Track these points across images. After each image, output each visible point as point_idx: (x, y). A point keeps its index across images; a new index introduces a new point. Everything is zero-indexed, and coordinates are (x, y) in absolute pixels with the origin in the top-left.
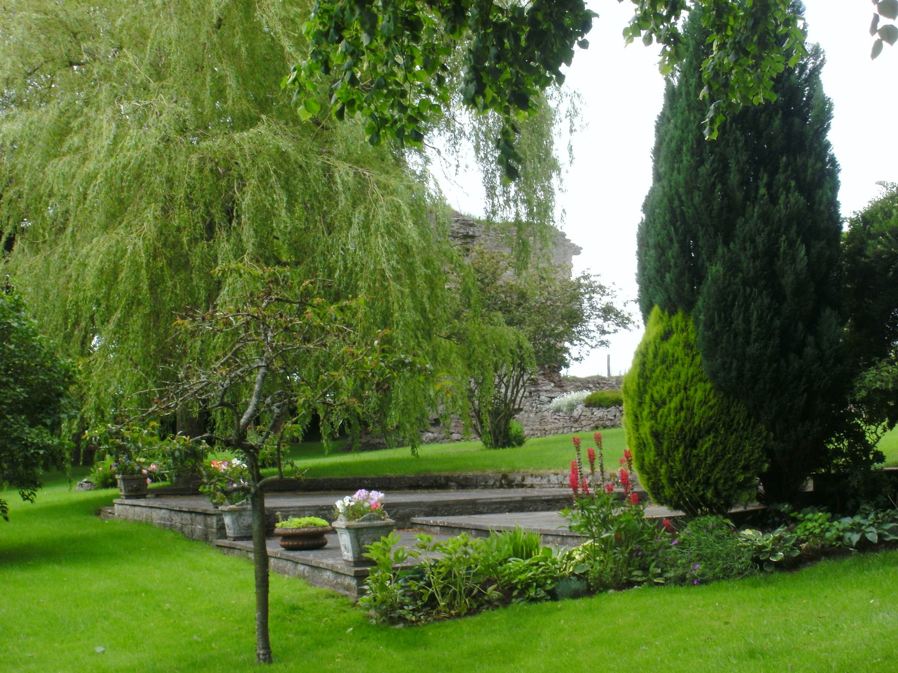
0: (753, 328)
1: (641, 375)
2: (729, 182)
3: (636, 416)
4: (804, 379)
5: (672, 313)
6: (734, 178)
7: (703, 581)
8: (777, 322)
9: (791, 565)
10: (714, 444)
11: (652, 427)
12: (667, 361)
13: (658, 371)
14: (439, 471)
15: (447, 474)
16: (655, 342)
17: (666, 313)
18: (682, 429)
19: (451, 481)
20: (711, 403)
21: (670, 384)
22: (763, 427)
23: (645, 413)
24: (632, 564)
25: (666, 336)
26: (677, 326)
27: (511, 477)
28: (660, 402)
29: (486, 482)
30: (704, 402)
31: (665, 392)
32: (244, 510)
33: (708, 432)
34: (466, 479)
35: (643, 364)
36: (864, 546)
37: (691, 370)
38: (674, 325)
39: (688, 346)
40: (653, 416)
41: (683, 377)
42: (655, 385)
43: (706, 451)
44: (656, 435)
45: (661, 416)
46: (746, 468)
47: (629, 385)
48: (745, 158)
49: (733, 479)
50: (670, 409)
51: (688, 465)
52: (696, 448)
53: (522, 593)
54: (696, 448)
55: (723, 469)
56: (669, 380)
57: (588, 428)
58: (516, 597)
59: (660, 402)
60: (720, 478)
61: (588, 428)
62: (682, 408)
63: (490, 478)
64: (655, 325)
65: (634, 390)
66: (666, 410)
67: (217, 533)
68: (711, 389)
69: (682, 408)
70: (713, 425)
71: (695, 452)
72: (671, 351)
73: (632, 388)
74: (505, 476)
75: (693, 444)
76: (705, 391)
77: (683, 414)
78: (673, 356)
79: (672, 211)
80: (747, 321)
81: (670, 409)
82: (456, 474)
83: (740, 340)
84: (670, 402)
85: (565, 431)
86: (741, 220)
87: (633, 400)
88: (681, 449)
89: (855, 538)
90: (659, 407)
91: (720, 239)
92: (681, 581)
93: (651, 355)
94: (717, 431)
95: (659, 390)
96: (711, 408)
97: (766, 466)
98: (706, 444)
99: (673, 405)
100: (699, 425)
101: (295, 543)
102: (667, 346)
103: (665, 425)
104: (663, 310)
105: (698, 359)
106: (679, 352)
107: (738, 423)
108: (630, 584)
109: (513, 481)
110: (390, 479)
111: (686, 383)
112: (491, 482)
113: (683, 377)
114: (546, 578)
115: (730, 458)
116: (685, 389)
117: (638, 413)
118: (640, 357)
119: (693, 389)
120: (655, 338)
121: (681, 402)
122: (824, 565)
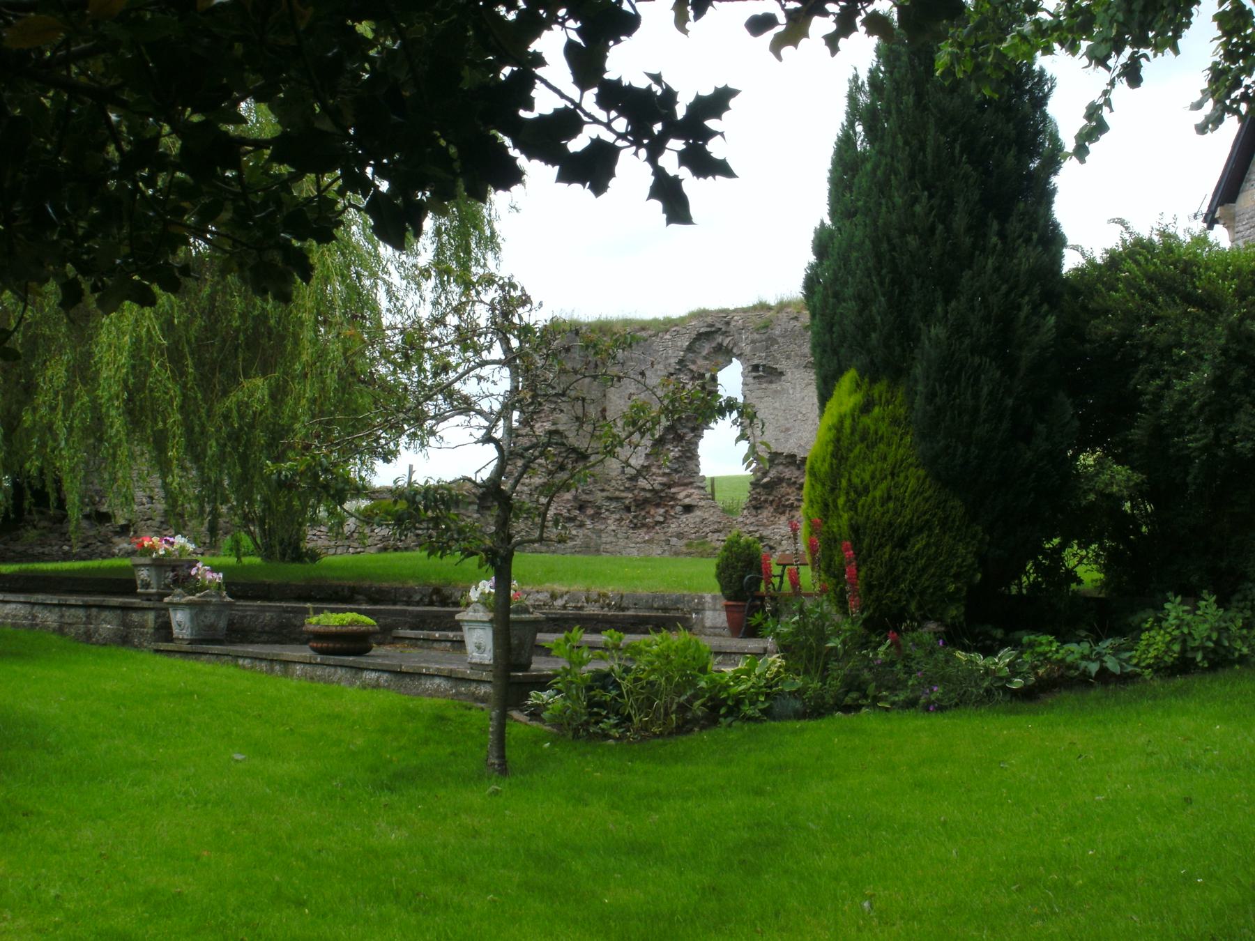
0: (983, 406)
1: (834, 455)
2: (954, 225)
3: (826, 505)
4: (1033, 475)
5: (873, 381)
6: (960, 221)
7: (941, 709)
8: (1010, 402)
9: (1029, 695)
10: (927, 545)
11: (851, 519)
12: (868, 439)
13: (856, 451)
14: (338, 579)
15: (351, 583)
16: (853, 416)
17: (866, 380)
18: (890, 524)
19: (359, 593)
20: (927, 494)
21: (872, 467)
22: (979, 528)
23: (841, 501)
24: (833, 689)
25: (866, 408)
26: (880, 397)
27: (446, 591)
28: (860, 488)
29: (410, 597)
30: (915, 494)
31: (867, 477)
32: (208, 603)
33: (920, 531)
34: (380, 591)
35: (837, 440)
36: (1104, 676)
37: (901, 451)
38: (876, 395)
39: (895, 422)
40: (852, 505)
41: (890, 459)
42: (853, 467)
43: (917, 553)
44: (855, 529)
45: (863, 506)
46: (957, 577)
47: (817, 465)
48: (977, 197)
49: (942, 588)
50: (874, 498)
51: (892, 569)
52: (904, 548)
53: (730, 712)
54: (904, 548)
55: (933, 576)
56: (872, 462)
57: (373, 550)
58: (725, 716)
59: (860, 488)
60: (928, 587)
61: (373, 550)
62: (889, 498)
63: (416, 592)
64: (850, 394)
65: (826, 473)
66: (869, 499)
67: (154, 634)
68: (926, 477)
69: (889, 498)
70: (927, 521)
71: (903, 554)
72: (873, 428)
73: (823, 470)
74: (437, 591)
75: (902, 543)
76: (918, 479)
77: (891, 505)
78: (876, 433)
79: (879, 257)
80: (976, 396)
81: (874, 498)
82: (367, 584)
83: (966, 418)
84: (875, 488)
85: (339, 551)
86: (967, 274)
87: (823, 485)
88: (887, 549)
89: (1094, 668)
90: (859, 495)
91: (939, 294)
92: (911, 704)
93: (847, 430)
94: (931, 529)
95: (860, 475)
96: (927, 500)
97: (979, 576)
98: (919, 543)
99: (878, 494)
100: (911, 520)
101: (338, 645)
102: (866, 420)
103: (868, 518)
104: (862, 376)
105: (908, 439)
106: (883, 428)
107: (954, 521)
108: (855, 708)
109: (448, 598)
110: (269, 586)
111: (894, 467)
112: (417, 597)
113: (890, 459)
114: (757, 694)
115: (942, 563)
116: (893, 474)
117: (830, 500)
118: (834, 431)
119: (902, 475)
120: (853, 410)
121: (889, 489)
122: (1069, 697)
